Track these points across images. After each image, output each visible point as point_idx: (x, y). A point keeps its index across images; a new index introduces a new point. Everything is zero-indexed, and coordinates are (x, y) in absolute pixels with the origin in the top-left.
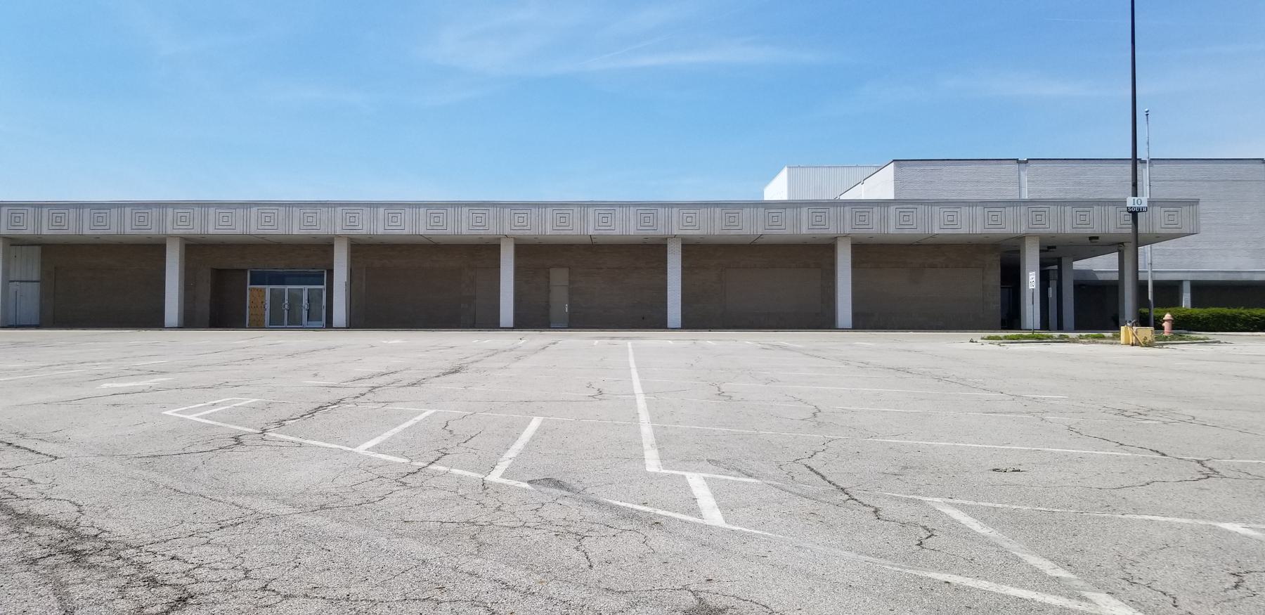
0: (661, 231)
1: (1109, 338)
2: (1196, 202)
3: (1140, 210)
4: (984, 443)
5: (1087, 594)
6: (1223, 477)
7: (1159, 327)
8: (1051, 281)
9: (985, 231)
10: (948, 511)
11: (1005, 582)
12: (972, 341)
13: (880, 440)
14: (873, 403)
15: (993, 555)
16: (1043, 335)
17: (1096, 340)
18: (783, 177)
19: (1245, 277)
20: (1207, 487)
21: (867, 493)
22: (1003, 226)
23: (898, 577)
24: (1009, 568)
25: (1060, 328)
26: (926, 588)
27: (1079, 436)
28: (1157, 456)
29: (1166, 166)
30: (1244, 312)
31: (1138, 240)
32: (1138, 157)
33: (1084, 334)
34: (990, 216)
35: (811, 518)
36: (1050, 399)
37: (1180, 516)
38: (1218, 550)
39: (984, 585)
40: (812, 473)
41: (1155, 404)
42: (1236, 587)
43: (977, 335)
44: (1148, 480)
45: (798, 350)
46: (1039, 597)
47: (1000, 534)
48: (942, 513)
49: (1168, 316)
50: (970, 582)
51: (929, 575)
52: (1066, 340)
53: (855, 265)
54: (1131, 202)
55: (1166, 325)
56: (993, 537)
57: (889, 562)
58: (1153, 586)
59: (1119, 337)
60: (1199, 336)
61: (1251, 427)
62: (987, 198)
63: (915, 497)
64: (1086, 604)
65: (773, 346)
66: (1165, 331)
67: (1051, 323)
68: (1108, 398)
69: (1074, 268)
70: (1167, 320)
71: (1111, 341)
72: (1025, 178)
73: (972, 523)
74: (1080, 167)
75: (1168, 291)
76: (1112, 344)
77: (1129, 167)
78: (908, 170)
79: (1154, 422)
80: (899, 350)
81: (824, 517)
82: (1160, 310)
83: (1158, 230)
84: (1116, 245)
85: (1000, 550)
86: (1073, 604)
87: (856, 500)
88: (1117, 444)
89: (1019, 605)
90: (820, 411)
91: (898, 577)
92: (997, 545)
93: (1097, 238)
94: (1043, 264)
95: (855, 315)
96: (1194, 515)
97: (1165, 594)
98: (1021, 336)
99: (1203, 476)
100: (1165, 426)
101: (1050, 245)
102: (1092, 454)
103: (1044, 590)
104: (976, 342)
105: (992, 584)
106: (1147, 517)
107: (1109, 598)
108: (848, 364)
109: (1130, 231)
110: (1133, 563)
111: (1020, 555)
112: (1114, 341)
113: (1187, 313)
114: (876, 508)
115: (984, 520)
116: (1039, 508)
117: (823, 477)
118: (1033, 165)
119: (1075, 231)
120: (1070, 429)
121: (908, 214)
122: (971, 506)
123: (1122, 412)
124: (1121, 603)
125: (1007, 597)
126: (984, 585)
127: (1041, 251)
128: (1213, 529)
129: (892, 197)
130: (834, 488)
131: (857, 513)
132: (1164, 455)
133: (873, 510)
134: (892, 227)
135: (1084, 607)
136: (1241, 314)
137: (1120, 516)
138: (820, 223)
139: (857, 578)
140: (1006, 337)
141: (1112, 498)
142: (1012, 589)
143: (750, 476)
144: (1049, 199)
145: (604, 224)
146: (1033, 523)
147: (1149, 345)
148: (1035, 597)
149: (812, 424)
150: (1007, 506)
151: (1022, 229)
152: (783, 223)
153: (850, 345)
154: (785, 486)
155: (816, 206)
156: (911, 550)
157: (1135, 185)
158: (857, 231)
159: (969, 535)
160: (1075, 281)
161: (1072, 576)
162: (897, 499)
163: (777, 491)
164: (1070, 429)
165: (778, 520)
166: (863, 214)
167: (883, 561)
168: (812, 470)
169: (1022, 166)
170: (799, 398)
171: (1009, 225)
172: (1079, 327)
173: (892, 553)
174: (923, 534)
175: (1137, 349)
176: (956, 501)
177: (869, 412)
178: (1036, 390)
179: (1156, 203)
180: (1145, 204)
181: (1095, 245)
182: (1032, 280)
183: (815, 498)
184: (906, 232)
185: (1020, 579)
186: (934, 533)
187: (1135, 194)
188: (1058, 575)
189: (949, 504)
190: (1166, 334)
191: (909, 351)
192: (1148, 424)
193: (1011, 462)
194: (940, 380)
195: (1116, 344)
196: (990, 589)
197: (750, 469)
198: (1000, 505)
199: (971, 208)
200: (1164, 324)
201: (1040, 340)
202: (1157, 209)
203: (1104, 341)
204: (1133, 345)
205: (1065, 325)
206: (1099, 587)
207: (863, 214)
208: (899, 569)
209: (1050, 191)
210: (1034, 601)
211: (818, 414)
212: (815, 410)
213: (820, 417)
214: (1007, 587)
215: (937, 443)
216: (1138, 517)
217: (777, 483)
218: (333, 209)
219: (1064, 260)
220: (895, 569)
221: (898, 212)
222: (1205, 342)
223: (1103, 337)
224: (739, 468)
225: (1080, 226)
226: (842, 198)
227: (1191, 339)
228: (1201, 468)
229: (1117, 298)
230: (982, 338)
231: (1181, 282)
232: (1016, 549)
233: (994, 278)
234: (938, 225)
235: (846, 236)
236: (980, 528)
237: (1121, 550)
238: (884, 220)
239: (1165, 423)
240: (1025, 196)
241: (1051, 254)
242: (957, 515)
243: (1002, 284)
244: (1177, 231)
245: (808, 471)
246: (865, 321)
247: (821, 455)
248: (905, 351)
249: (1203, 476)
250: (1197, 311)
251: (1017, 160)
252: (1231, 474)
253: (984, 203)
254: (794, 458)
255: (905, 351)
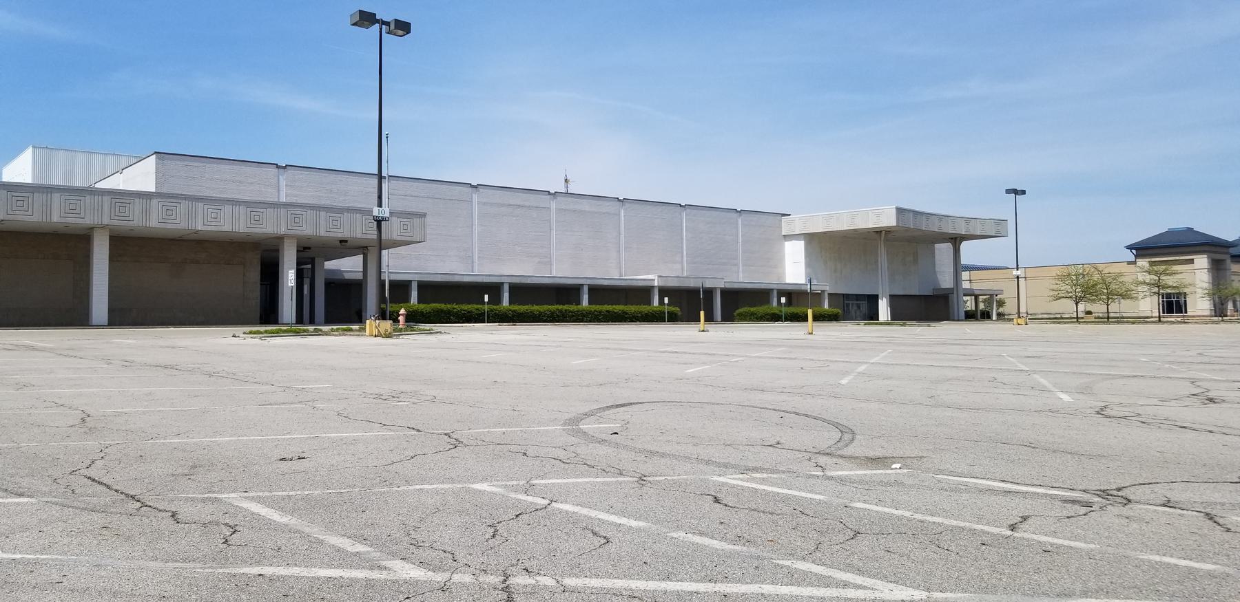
0: (88, 220)
1: (356, 330)
2: (424, 215)
3: (383, 219)
4: (267, 435)
5: (384, 563)
6: (466, 446)
7: (396, 321)
8: (305, 279)
9: (247, 230)
10: (246, 505)
11: (314, 565)
12: (234, 336)
13: (162, 441)
14: (146, 403)
15: (298, 541)
16: (300, 329)
17: (346, 333)
18: (27, 155)
19: (457, 279)
20: (456, 455)
21: (160, 497)
22: (264, 226)
23: (211, 578)
24: (314, 552)
25: (312, 322)
26: (242, 584)
27: (349, 420)
28: (414, 432)
29: (401, 182)
30: (456, 307)
31: (381, 245)
32: (383, 175)
33: (335, 327)
34: (252, 216)
35: (104, 532)
36: (318, 388)
37: (443, 482)
38: (475, 508)
39: (295, 571)
40: (94, 483)
41: (404, 387)
42: (494, 536)
43: (239, 330)
44: (412, 454)
45: (50, 350)
46: (346, 573)
47: (299, 520)
48: (241, 508)
49: (402, 311)
50: (282, 571)
51: (242, 571)
52: (320, 333)
53: (113, 258)
54: (376, 211)
55: (401, 318)
56: (293, 525)
57: (198, 565)
58: (435, 546)
59: (364, 329)
60: (426, 328)
61: (477, 402)
62: (248, 198)
63: (211, 495)
64: (386, 572)
65: (17, 345)
66: (400, 323)
67: (305, 317)
68: (366, 385)
69: (325, 268)
70: (401, 315)
71: (358, 333)
72: (283, 183)
73: (271, 514)
74: (332, 176)
75: (400, 289)
76: (359, 335)
77: (376, 181)
78: (170, 164)
79: (406, 403)
80: (161, 347)
81: (118, 529)
82: (394, 305)
83: (395, 237)
84: (361, 248)
85: (304, 536)
86: (375, 575)
87: (150, 506)
88: (381, 425)
89: (330, 584)
90: (89, 416)
91: (211, 578)
92: (299, 531)
93: (346, 241)
94: (299, 263)
95: (722, 318)
96: (453, 481)
97: (445, 552)
98: (281, 330)
99: (452, 447)
100: (415, 406)
101: (306, 246)
102: (363, 435)
103: (349, 566)
104: (238, 337)
105: (303, 569)
106: (418, 487)
107: (403, 563)
108: (111, 363)
109: (375, 237)
110: (416, 529)
111: (321, 537)
112: (361, 333)
113: (415, 308)
114: (173, 512)
115: (282, 509)
116: (328, 491)
117: (108, 487)
118: (290, 171)
119: (328, 234)
120: (339, 414)
121: (172, 208)
122: (267, 497)
123: (379, 396)
124: (414, 566)
125: (318, 578)
126: (295, 571)
127: (298, 251)
128: (468, 491)
129: (153, 190)
130: (122, 496)
131: (154, 519)
132: (419, 431)
133: (170, 514)
134: (155, 221)
135: (384, 575)
136: (454, 309)
137: (396, 489)
138: (74, 212)
139: (169, 587)
140: (266, 332)
141: (387, 474)
142: (321, 570)
143: (21, 495)
144: (178, 194)
145: (213, 220)
146: (326, 506)
147: (389, 336)
148: (343, 574)
149: (82, 430)
150: (299, 492)
151: (282, 230)
152: (30, 209)
153: (107, 343)
154: (66, 502)
155: (122, 196)
156: (218, 549)
157: (380, 197)
158: (116, 223)
159: (269, 523)
160: (325, 279)
161: (369, 549)
162: (193, 499)
163: (58, 508)
164: (339, 414)
165: (66, 541)
166: (124, 205)
167: (192, 565)
168: (94, 480)
169: (281, 170)
170: (61, 403)
171: (269, 225)
172: (329, 321)
173: (200, 555)
174: (227, 532)
175: (379, 340)
176: (251, 494)
177: (144, 413)
178: (303, 381)
179: (394, 214)
180: (387, 215)
181: (344, 248)
182: (289, 278)
183: (103, 511)
184: (169, 226)
185: (326, 559)
186: (237, 528)
187: (380, 205)
188: (357, 550)
189: (245, 497)
190: (401, 326)
191: (173, 347)
192: (401, 405)
193: (293, 451)
194: (210, 376)
195: (362, 335)
196: (302, 574)
197: (20, 488)
198: (293, 493)
199: (234, 207)
200: (399, 318)
201: (297, 333)
202: (394, 219)
203: (351, 333)
204: (375, 336)
205: (316, 320)
206: (393, 555)
207: (124, 205)
208: (211, 570)
209: (306, 195)
210: (343, 578)
211: (88, 419)
212: (83, 416)
213: (90, 422)
214: (317, 570)
215: (221, 439)
216: (411, 488)
217: (56, 500)
218: (100, 197)
219: (317, 260)
220: (207, 570)
221: (160, 206)
222: (430, 332)
223: (351, 330)
224: (5, 487)
225: (332, 230)
226: (98, 186)
227: (420, 330)
228: (449, 440)
229: (361, 296)
230: (244, 333)
231: (410, 282)
232: (316, 532)
233: (255, 275)
234: (202, 222)
235: (104, 227)
236: (279, 517)
237: (404, 519)
238: (146, 212)
239: (414, 403)
240: (283, 199)
241: (307, 254)
242: (255, 507)
243: (261, 281)
244: (409, 239)
245: (89, 482)
246: (121, 317)
247: (99, 463)
248: (168, 347)
249: (452, 447)
250: (422, 306)
251: (277, 164)
252: (471, 442)
253: (247, 203)
254: (70, 470)
255: (168, 347)
